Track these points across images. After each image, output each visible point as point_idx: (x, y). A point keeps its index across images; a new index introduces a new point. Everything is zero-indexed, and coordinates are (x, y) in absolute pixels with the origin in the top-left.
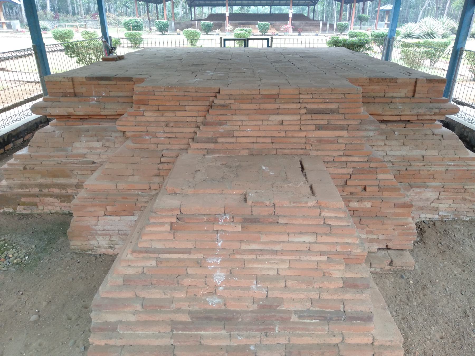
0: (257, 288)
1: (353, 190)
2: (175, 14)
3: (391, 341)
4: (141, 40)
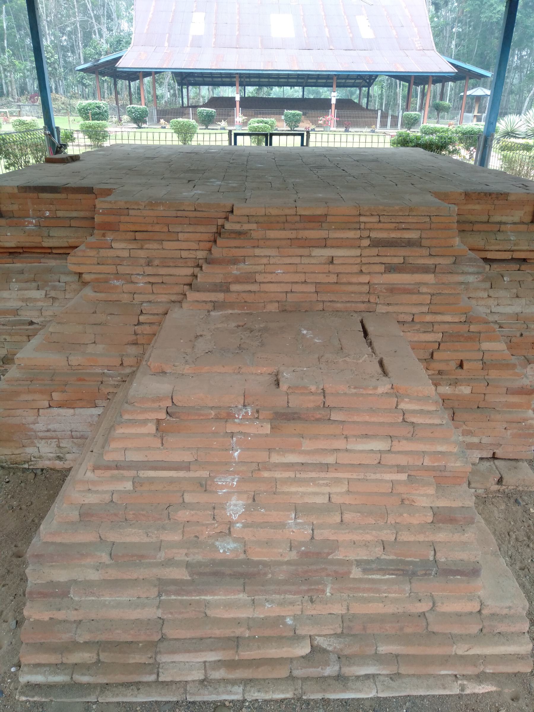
0: (297, 524)
1: (442, 366)
2: (157, 97)
3: (510, 608)
4: (105, 136)
